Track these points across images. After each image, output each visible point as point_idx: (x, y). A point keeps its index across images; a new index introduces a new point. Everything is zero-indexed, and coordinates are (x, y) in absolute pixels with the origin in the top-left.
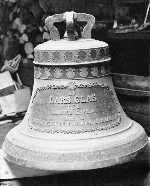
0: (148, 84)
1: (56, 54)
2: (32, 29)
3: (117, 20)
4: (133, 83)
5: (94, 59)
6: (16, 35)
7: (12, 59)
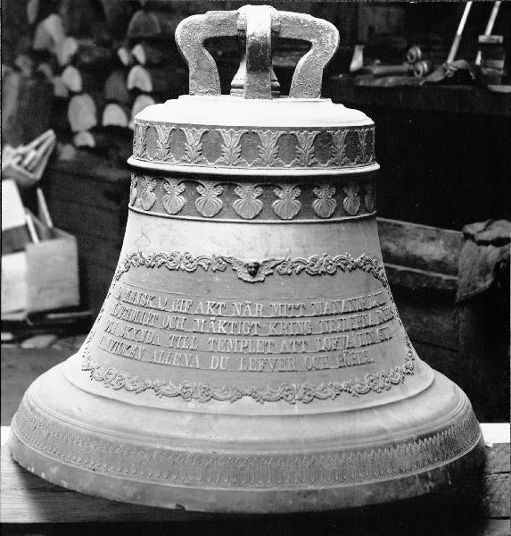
0: (444, 252)
1: (211, 140)
2: (97, 53)
3: (363, 47)
4: (397, 245)
5: (325, 163)
6: (45, 68)
7: (27, 141)
